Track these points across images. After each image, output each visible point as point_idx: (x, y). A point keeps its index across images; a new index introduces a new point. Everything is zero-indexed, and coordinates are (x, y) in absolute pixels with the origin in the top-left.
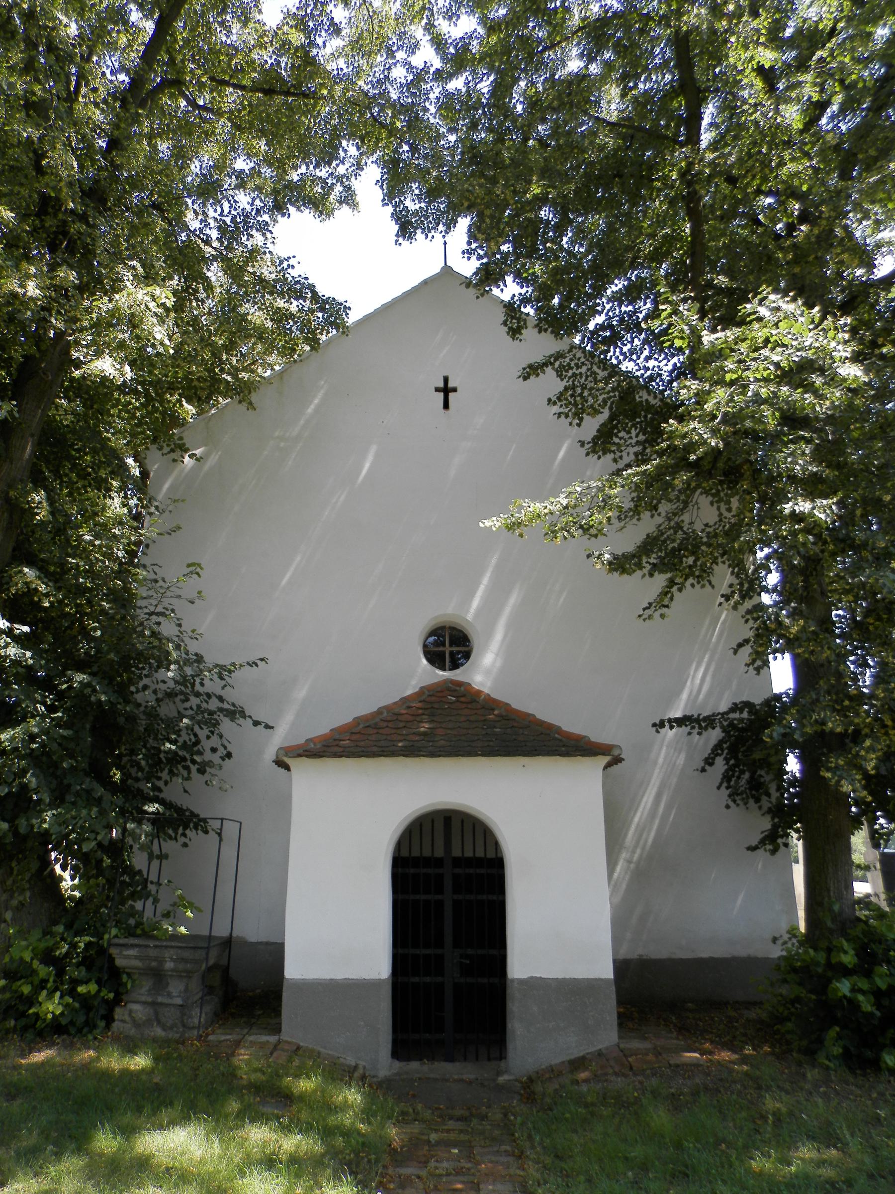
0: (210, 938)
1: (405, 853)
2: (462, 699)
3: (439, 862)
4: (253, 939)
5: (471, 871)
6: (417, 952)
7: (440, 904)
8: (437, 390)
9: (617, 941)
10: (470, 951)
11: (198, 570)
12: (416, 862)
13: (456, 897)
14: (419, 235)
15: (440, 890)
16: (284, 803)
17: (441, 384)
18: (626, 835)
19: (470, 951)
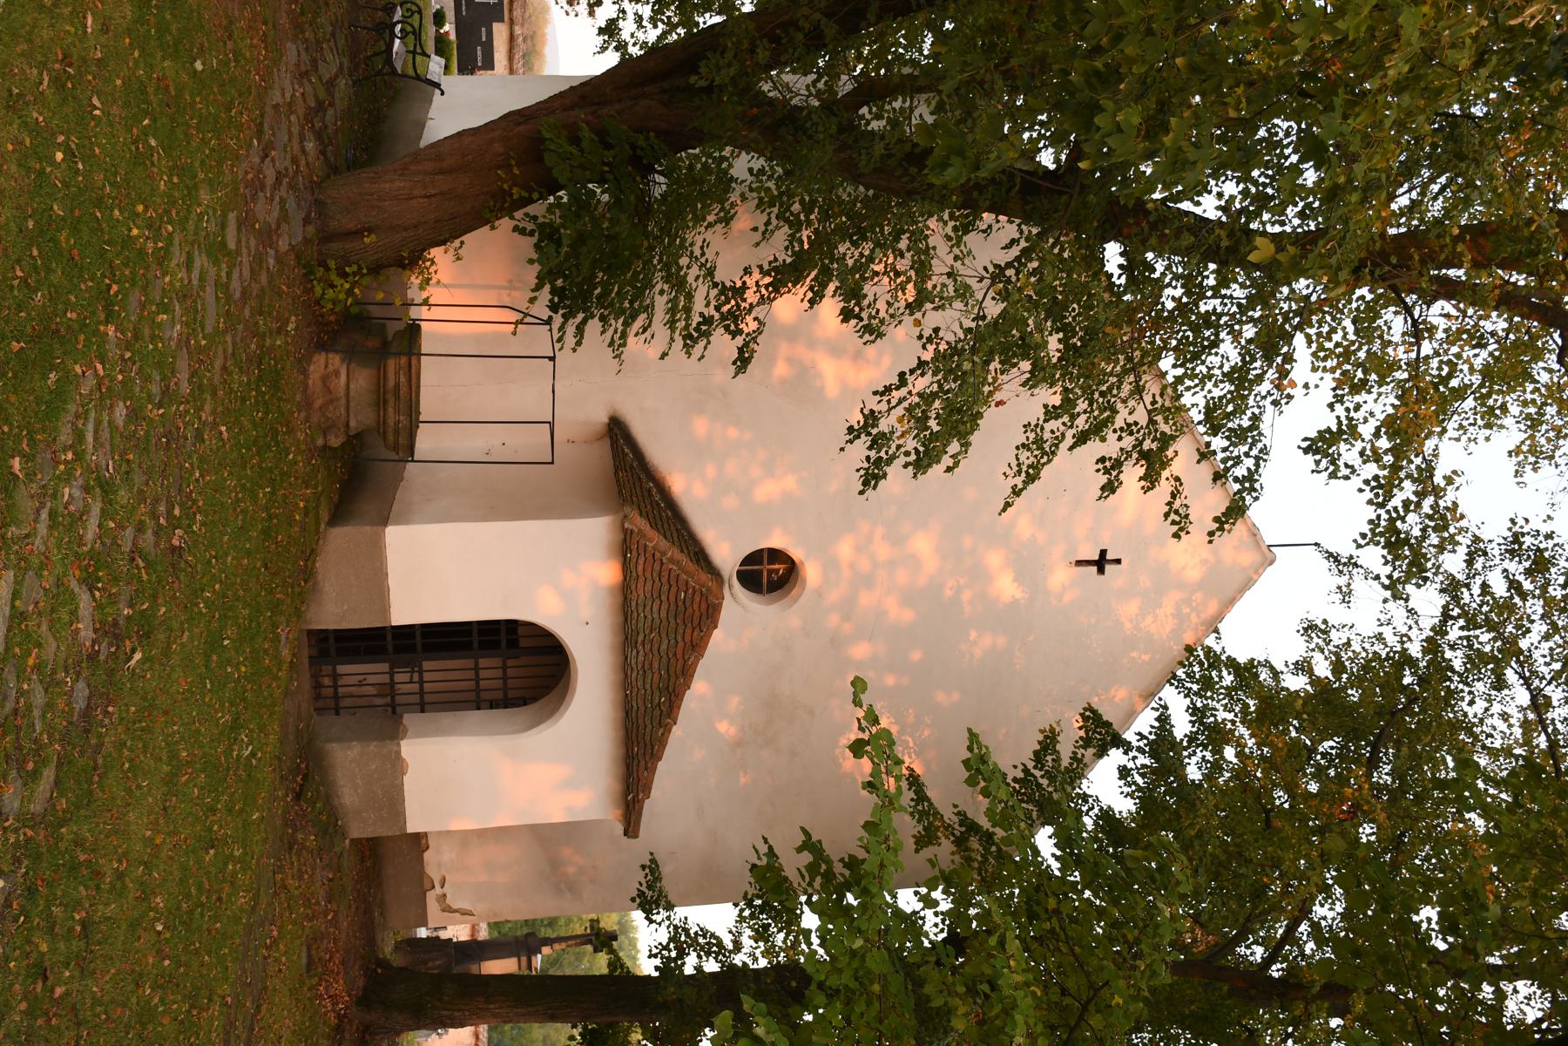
1: (521, 631)
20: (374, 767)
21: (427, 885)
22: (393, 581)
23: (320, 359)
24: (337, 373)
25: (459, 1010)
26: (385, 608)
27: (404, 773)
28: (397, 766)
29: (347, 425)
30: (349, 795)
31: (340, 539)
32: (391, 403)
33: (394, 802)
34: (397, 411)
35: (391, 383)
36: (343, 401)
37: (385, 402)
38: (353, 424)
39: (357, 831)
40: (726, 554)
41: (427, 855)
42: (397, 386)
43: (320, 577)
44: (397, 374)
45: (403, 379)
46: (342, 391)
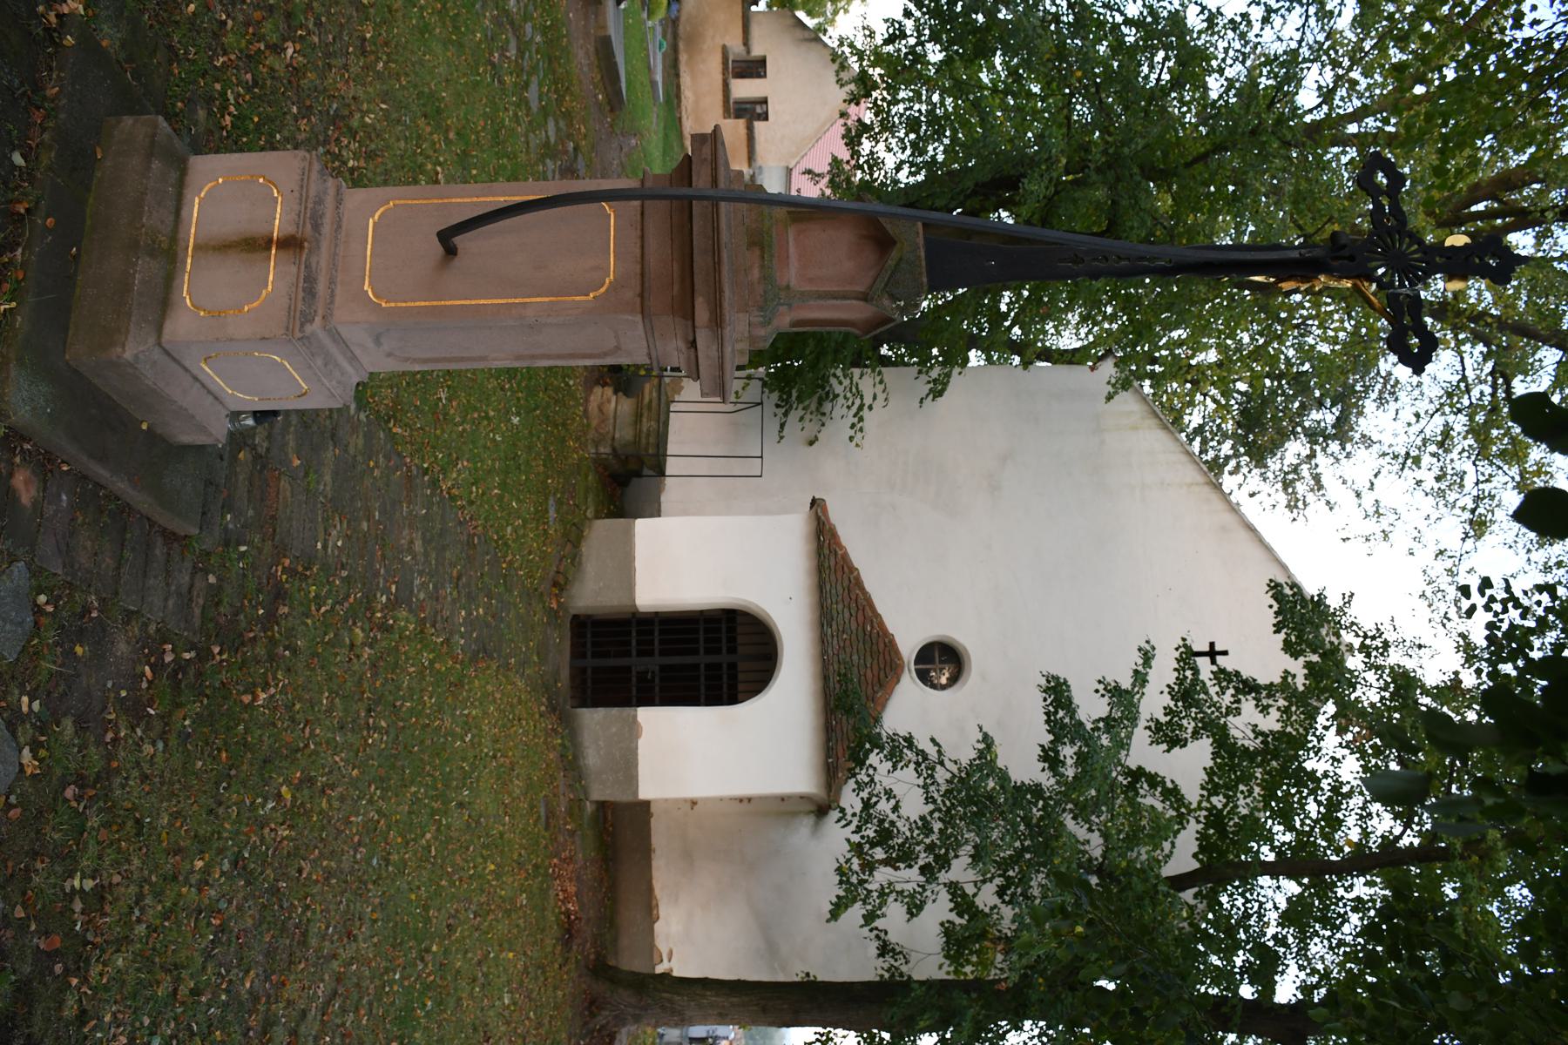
0: (665, 455)
1: (739, 619)
2: (882, 673)
3: (732, 650)
4: (663, 499)
5: (725, 689)
6: (656, 633)
7: (695, 652)
8: (1212, 645)
9: (656, 801)
10: (657, 680)
11: (843, 822)
12: (732, 630)
13: (702, 666)
14: (1306, 671)
15: (708, 651)
16: (784, 511)
17: (1218, 648)
18: (664, 67)
19: (657, 680)
20: (614, 730)
21: (656, 959)
22: (638, 564)
23: (598, 390)
24: (609, 401)
25: (679, 994)
26: (636, 792)
27: (638, 736)
28: (634, 730)
29: (613, 439)
30: (592, 758)
31: (602, 530)
32: (645, 414)
33: (627, 766)
34: (649, 420)
35: (646, 400)
36: (612, 421)
37: (641, 415)
38: (617, 436)
39: (597, 794)
40: (908, 646)
41: (657, 926)
42: (651, 401)
43: (584, 559)
44: (651, 392)
45: (655, 394)
46: (612, 415)
